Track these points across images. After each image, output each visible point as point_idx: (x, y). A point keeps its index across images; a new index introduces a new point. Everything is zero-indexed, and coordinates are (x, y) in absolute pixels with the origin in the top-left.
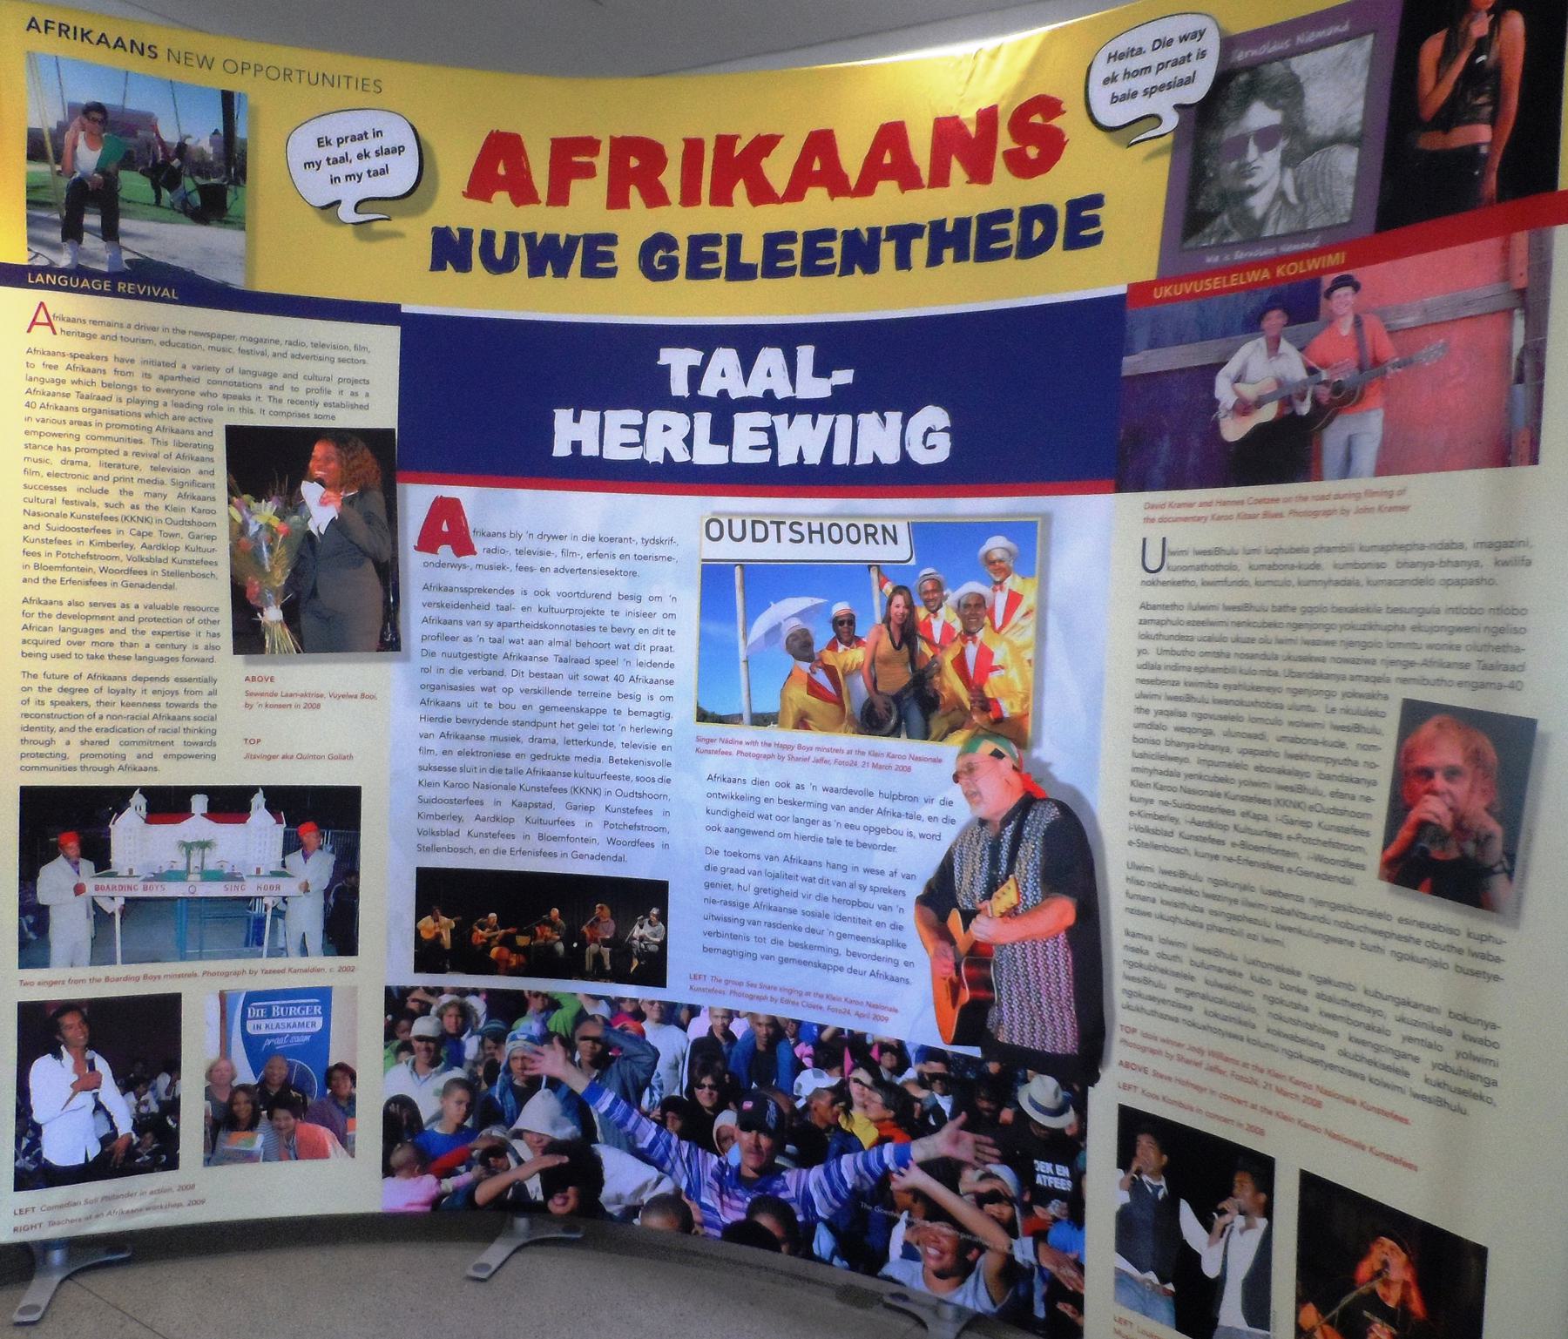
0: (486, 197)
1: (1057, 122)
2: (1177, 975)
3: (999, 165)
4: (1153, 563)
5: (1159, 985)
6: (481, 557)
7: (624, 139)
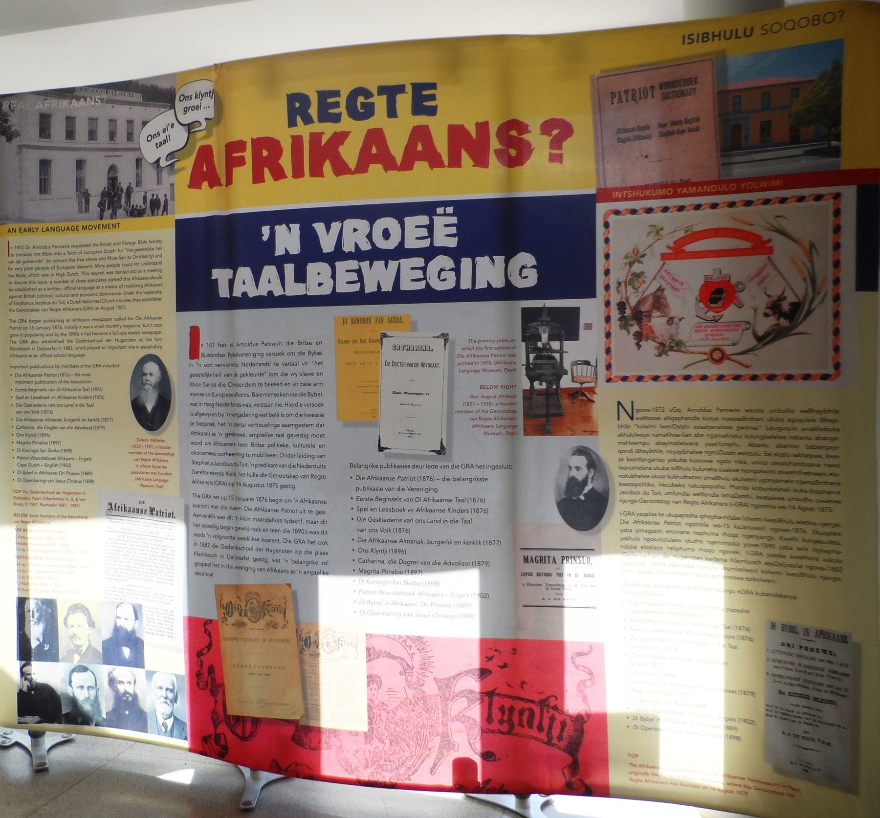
1: (526, 137)
3: (493, 159)
6: (202, 360)
7: (293, 95)
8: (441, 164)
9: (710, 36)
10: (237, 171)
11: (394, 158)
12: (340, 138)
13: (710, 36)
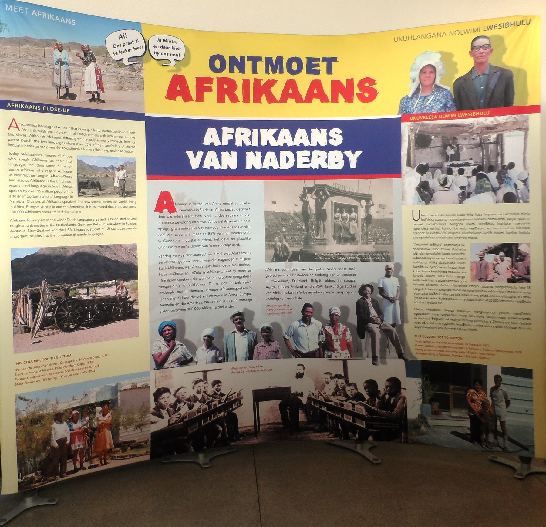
0: (174, 99)
1: (374, 87)
2: (452, 281)
3: (355, 98)
4: (416, 217)
5: (451, 277)
6: (178, 213)
8: (327, 101)
9: (510, 24)
10: (206, 95)
11: (301, 96)
12: (272, 83)
13: (510, 24)
